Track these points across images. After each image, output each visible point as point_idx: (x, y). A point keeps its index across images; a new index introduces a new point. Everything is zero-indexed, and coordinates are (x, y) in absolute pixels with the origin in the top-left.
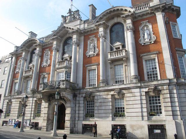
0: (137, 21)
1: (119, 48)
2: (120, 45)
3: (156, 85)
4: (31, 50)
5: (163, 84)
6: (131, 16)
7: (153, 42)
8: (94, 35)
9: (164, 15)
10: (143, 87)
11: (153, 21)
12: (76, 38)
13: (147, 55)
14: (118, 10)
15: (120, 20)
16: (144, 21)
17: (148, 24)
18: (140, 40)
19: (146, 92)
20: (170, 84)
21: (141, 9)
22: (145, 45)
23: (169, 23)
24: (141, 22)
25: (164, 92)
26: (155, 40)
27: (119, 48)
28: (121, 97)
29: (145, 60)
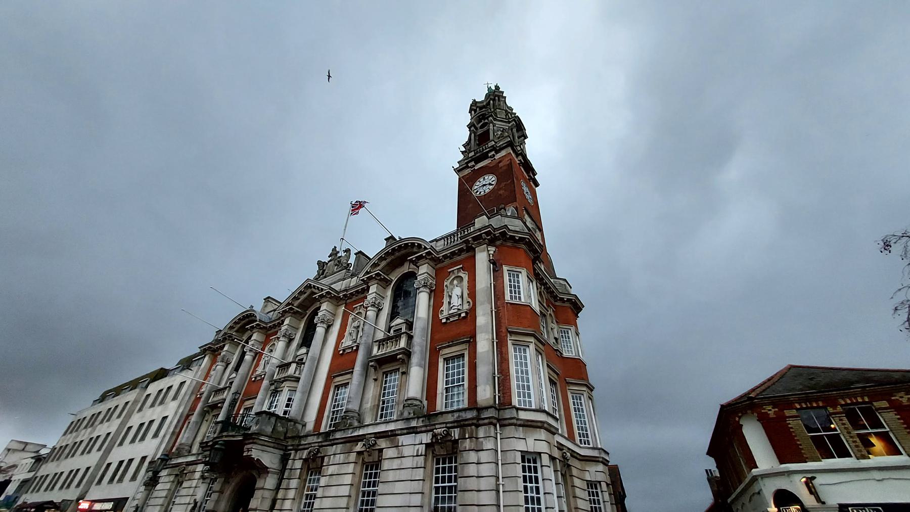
0: (442, 268)
4: (394, 277)
7: (463, 315)
29: (444, 359)
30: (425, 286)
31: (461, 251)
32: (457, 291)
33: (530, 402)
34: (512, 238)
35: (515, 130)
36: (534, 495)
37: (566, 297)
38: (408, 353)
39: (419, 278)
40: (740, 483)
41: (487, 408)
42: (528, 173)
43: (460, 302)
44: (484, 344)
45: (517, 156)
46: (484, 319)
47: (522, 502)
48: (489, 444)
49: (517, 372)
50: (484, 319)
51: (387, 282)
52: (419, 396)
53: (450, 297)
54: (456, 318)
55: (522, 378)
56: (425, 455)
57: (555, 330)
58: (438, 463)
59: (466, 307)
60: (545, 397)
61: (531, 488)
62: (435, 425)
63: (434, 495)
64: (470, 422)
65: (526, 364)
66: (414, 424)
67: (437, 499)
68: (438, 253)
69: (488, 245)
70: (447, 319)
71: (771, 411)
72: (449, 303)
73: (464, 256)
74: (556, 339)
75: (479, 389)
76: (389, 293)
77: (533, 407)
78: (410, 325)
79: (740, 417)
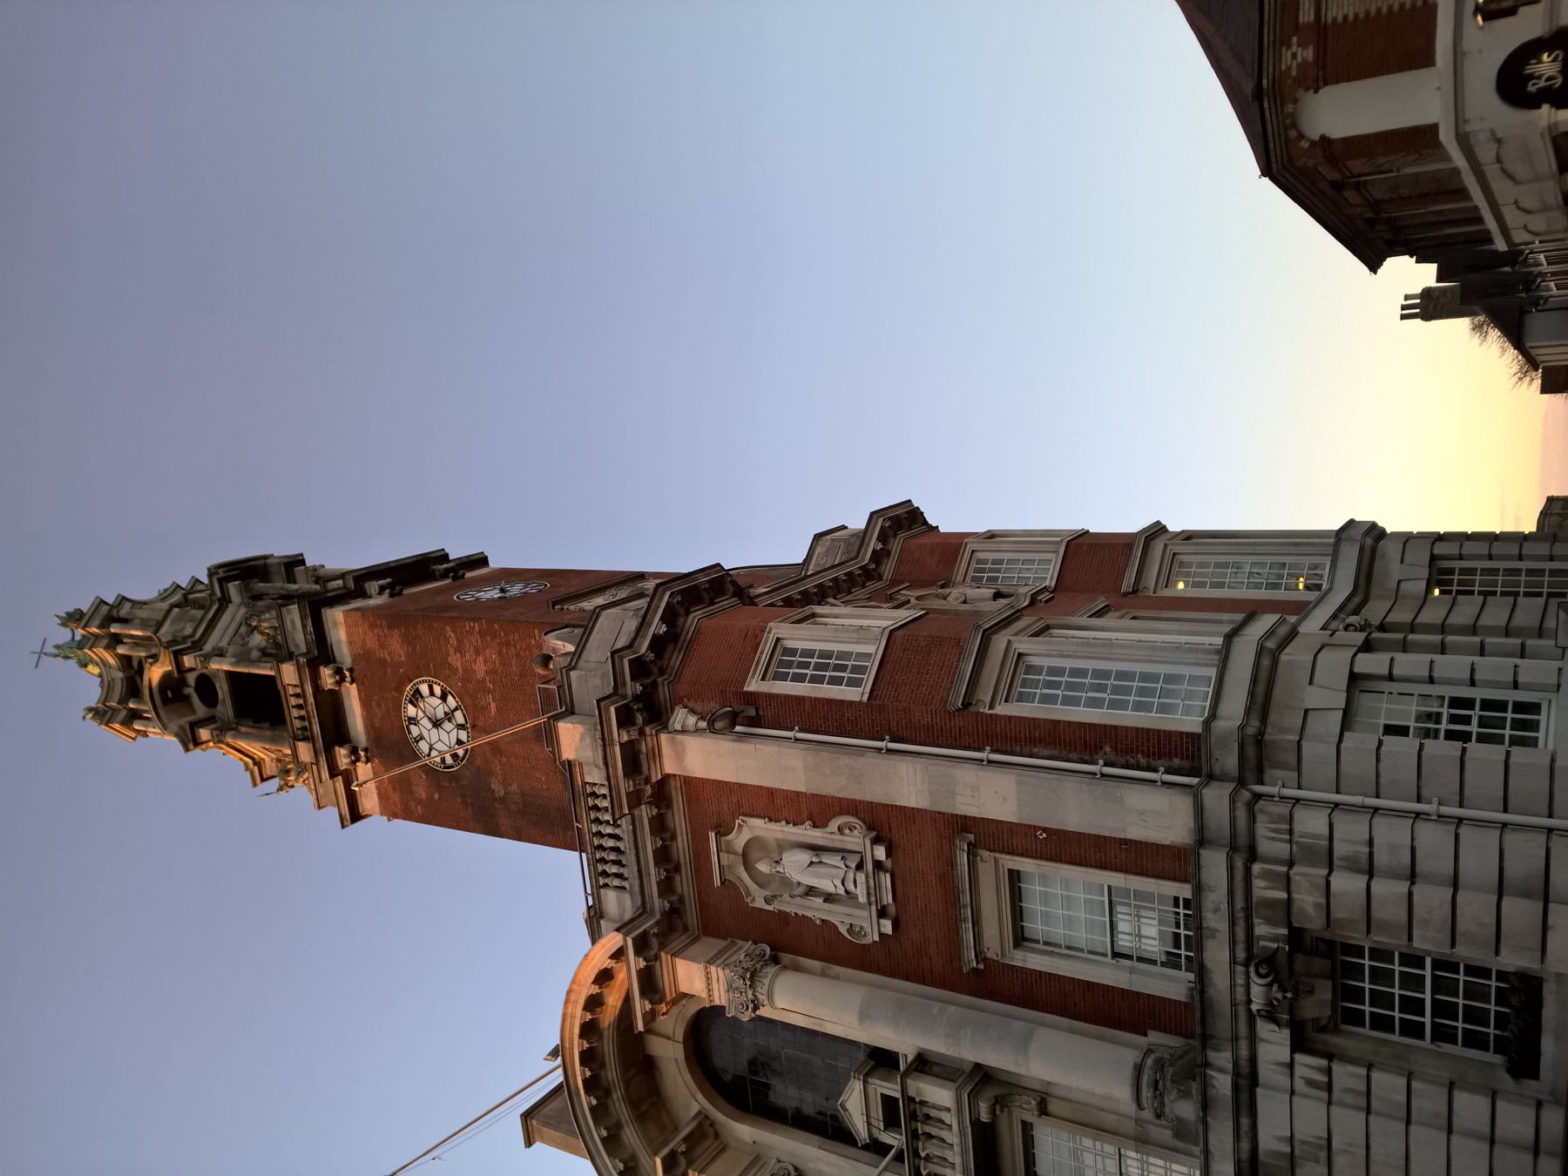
0: (703, 907)
1: (889, 1103)
2: (865, 1082)
3: (1241, 955)
5: (1231, 902)
6: (657, 957)
7: (880, 853)
8: (712, 835)
9: (692, 711)
10: (1244, 1052)
11: (724, 803)
12: (710, 962)
13: (976, 923)
14: (589, 1030)
15: (673, 1023)
16: (715, 859)
17: (739, 839)
18: (851, 929)
19: (1298, 1045)
20: (1243, 840)
21: (616, 850)
22: (892, 910)
23: (752, 698)
24: (717, 882)
25: (1311, 910)
26: (870, 828)
27: (889, 1103)
28: (1320, 964)
29: (1017, 945)
30: (753, 977)
31: (660, 826)
32: (795, 865)
33: (1194, 680)
34: (658, 644)
35: (260, 586)
36: (1475, 714)
37: (873, 544)
38: (982, 1077)
39: (720, 998)
40: (1462, 193)
41: (1199, 811)
42: (432, 577)
43: (835, 860)
44: (990, 791)
45: (364, 595)
46: (908, 780)
47: (1496, 752)
48: (1312, 823)
49: (1094, 703)
50: (908, 780)
51: (704, 1131)
52: (1131, 1057)
53: (811, 891)
54: (886, 880)
55: (1117, 690)
56: (1330, 1057)
57: (971, 592)
58: (1356, 1018)
59: (856, 839)
60: (1184, 639)
61: (1454, 719)
62: (1234, 1004)
63: (1458, 1050)
64: (1239, 876)
65: (1076, 672)
66: (1222, 1084)
67: (1473, 1040)
68: (643, 910)
69: (664, 726)
70: (882, 913)
71: (1299, 54)
72: (829, 898)
73: (679, 819)
74: (998, 595)
75: (1135, 833)
76: (744, 1131)
77: (1212, 672)
78: (882, 1060)
79: (1301, 136)
